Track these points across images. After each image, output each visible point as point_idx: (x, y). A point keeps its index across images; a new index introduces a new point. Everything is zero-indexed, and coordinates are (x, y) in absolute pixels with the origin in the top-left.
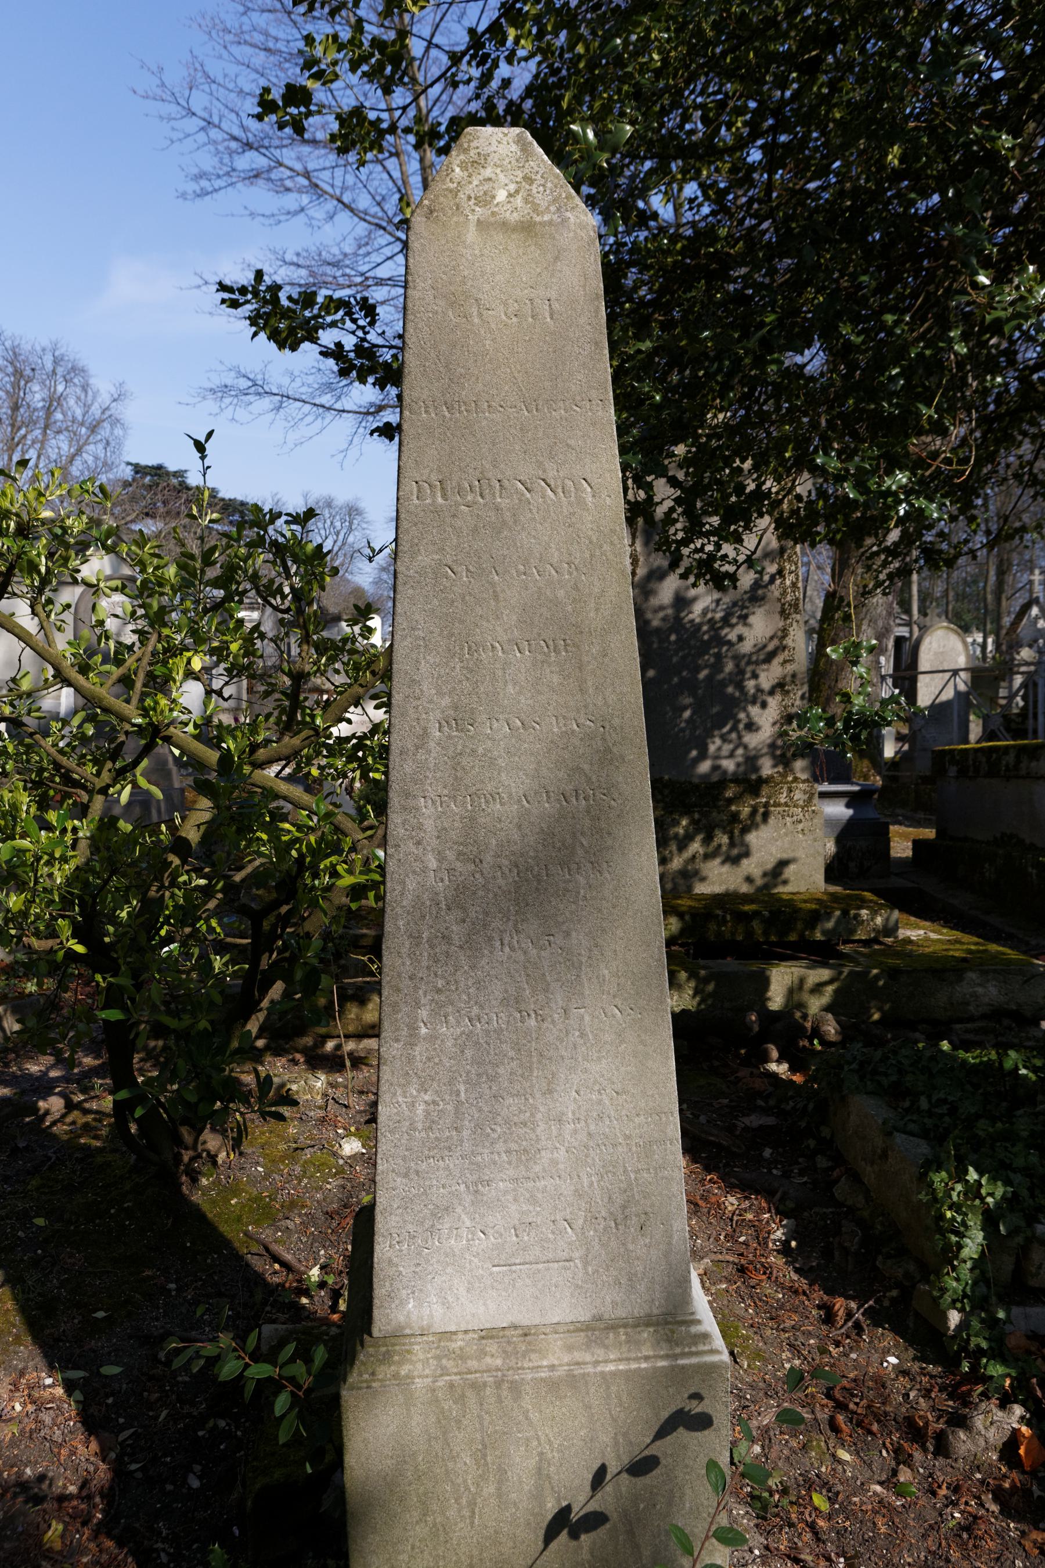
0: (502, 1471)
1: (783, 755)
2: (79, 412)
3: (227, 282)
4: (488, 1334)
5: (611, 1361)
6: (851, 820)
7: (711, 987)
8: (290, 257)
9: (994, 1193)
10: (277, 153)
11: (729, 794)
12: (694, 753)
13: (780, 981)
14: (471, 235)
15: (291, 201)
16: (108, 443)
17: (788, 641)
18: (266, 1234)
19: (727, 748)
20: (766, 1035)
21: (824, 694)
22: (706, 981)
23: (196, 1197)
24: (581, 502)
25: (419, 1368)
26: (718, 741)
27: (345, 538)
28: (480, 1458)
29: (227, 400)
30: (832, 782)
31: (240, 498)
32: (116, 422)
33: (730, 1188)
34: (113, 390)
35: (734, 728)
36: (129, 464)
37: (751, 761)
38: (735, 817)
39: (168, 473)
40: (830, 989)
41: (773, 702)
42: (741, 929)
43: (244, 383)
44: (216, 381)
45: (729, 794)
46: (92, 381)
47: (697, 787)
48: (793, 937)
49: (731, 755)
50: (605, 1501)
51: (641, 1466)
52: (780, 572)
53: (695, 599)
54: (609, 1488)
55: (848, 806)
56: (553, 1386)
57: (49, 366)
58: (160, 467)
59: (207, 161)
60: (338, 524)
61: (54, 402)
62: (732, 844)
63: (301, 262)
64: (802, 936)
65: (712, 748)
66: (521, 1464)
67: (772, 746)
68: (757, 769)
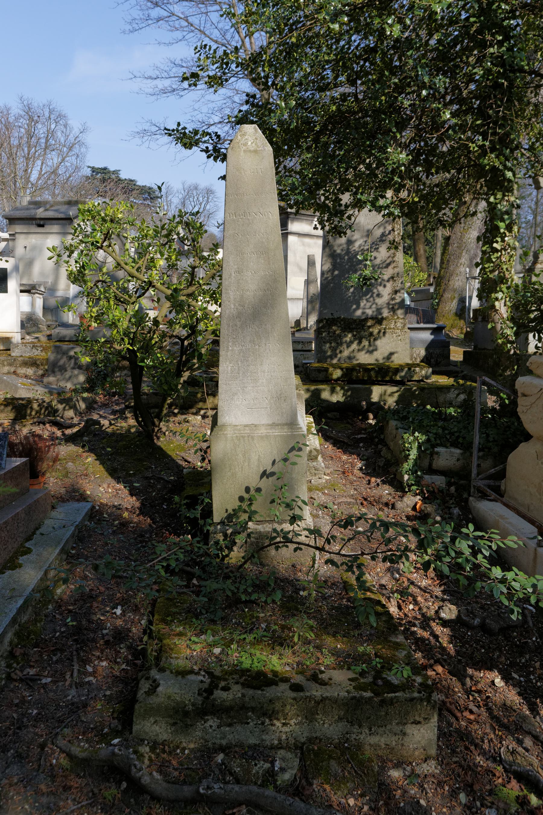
0: (249, 459)
1: (393, 308)
2: (62, 140)
3: (168, 127)
4: (246, 426)
5: (277, 432)
6: (432, 341)
7: (349, 393)
8: (178, 62)
9: (422, 438)
10: (171, 7)
11: (369, 324)
12: (354, 307)
13: (377, 392)
14: (242, 153)
15: (178, 34)
16: (78, 156)
17: (396, 259)
18: (183, 454)
19: (369, 304)
20: (368, 410)
21: (443, 287)
22: (347, 391)
23: (159, 444)
24: (269, 218)
25: (229, 432)
26: (365, 302)
27: (205, 207)
28: (244, 455)
29: (146, 138)
30: (425, 323)
31: (148, 185)
32: (81, 144)
33: (345, 452)
34: (80, 127)
35: (372, 296)
36: (89, 167)
37: (379, 310)
38: (371, 334)
39: (109, 172)
40: (396, 395)
41: (389, 285)
42: (366, 375)
43: (154, 129)
44: (140, 128)
45: (369, 324)
46: (69, 122)
47: (355, 320)
48: (387, 379)
49: (370, 308)
50: (275, 469)
51: (285, 460)
52: (393, 230)
53: (355, 241)
54: (276, 466)
55: (431, 334)
56: (262, 437)
57: (47, 114)
58: (105, 169)
59: (136, 13)
60: (201, 199)
61: (50, 134)
62: (370, 345)
63: (184, 65)
64: (391, 378)
65: (362, 304)
66: (254, 458)
67: (388, 304)
68: (381, 314)
